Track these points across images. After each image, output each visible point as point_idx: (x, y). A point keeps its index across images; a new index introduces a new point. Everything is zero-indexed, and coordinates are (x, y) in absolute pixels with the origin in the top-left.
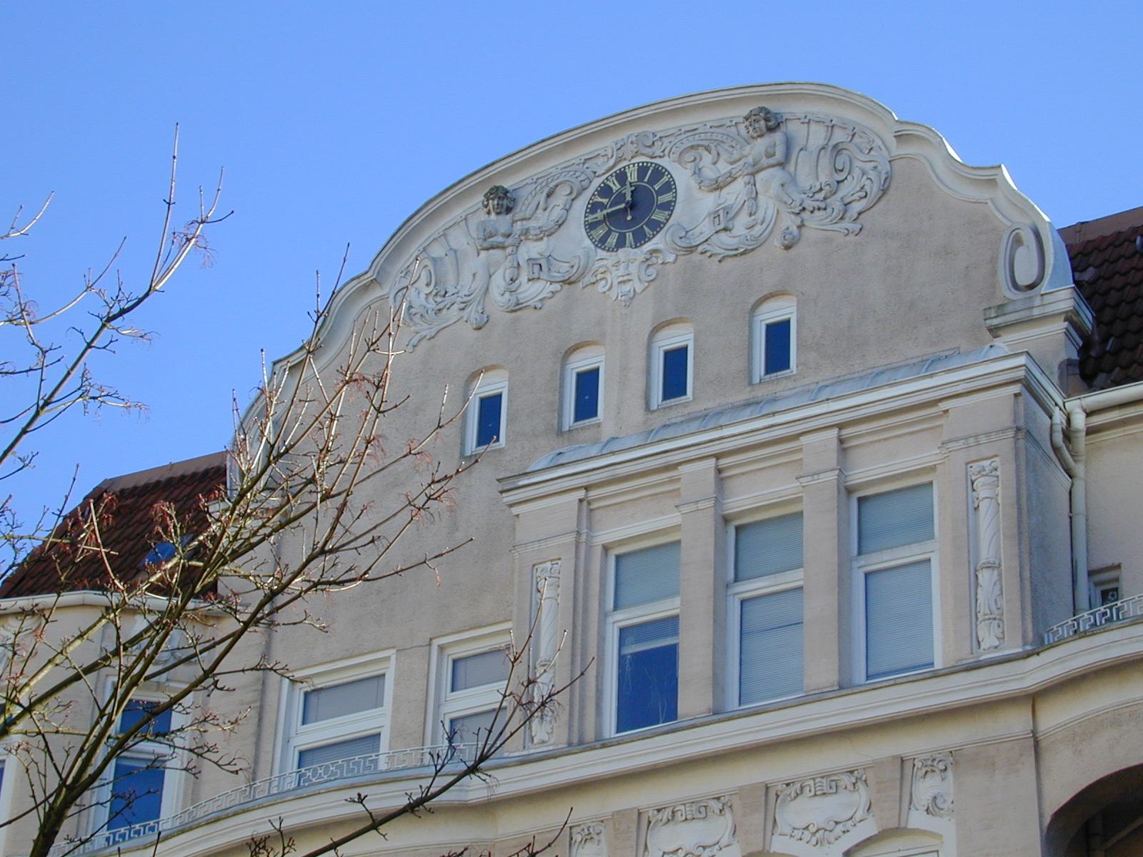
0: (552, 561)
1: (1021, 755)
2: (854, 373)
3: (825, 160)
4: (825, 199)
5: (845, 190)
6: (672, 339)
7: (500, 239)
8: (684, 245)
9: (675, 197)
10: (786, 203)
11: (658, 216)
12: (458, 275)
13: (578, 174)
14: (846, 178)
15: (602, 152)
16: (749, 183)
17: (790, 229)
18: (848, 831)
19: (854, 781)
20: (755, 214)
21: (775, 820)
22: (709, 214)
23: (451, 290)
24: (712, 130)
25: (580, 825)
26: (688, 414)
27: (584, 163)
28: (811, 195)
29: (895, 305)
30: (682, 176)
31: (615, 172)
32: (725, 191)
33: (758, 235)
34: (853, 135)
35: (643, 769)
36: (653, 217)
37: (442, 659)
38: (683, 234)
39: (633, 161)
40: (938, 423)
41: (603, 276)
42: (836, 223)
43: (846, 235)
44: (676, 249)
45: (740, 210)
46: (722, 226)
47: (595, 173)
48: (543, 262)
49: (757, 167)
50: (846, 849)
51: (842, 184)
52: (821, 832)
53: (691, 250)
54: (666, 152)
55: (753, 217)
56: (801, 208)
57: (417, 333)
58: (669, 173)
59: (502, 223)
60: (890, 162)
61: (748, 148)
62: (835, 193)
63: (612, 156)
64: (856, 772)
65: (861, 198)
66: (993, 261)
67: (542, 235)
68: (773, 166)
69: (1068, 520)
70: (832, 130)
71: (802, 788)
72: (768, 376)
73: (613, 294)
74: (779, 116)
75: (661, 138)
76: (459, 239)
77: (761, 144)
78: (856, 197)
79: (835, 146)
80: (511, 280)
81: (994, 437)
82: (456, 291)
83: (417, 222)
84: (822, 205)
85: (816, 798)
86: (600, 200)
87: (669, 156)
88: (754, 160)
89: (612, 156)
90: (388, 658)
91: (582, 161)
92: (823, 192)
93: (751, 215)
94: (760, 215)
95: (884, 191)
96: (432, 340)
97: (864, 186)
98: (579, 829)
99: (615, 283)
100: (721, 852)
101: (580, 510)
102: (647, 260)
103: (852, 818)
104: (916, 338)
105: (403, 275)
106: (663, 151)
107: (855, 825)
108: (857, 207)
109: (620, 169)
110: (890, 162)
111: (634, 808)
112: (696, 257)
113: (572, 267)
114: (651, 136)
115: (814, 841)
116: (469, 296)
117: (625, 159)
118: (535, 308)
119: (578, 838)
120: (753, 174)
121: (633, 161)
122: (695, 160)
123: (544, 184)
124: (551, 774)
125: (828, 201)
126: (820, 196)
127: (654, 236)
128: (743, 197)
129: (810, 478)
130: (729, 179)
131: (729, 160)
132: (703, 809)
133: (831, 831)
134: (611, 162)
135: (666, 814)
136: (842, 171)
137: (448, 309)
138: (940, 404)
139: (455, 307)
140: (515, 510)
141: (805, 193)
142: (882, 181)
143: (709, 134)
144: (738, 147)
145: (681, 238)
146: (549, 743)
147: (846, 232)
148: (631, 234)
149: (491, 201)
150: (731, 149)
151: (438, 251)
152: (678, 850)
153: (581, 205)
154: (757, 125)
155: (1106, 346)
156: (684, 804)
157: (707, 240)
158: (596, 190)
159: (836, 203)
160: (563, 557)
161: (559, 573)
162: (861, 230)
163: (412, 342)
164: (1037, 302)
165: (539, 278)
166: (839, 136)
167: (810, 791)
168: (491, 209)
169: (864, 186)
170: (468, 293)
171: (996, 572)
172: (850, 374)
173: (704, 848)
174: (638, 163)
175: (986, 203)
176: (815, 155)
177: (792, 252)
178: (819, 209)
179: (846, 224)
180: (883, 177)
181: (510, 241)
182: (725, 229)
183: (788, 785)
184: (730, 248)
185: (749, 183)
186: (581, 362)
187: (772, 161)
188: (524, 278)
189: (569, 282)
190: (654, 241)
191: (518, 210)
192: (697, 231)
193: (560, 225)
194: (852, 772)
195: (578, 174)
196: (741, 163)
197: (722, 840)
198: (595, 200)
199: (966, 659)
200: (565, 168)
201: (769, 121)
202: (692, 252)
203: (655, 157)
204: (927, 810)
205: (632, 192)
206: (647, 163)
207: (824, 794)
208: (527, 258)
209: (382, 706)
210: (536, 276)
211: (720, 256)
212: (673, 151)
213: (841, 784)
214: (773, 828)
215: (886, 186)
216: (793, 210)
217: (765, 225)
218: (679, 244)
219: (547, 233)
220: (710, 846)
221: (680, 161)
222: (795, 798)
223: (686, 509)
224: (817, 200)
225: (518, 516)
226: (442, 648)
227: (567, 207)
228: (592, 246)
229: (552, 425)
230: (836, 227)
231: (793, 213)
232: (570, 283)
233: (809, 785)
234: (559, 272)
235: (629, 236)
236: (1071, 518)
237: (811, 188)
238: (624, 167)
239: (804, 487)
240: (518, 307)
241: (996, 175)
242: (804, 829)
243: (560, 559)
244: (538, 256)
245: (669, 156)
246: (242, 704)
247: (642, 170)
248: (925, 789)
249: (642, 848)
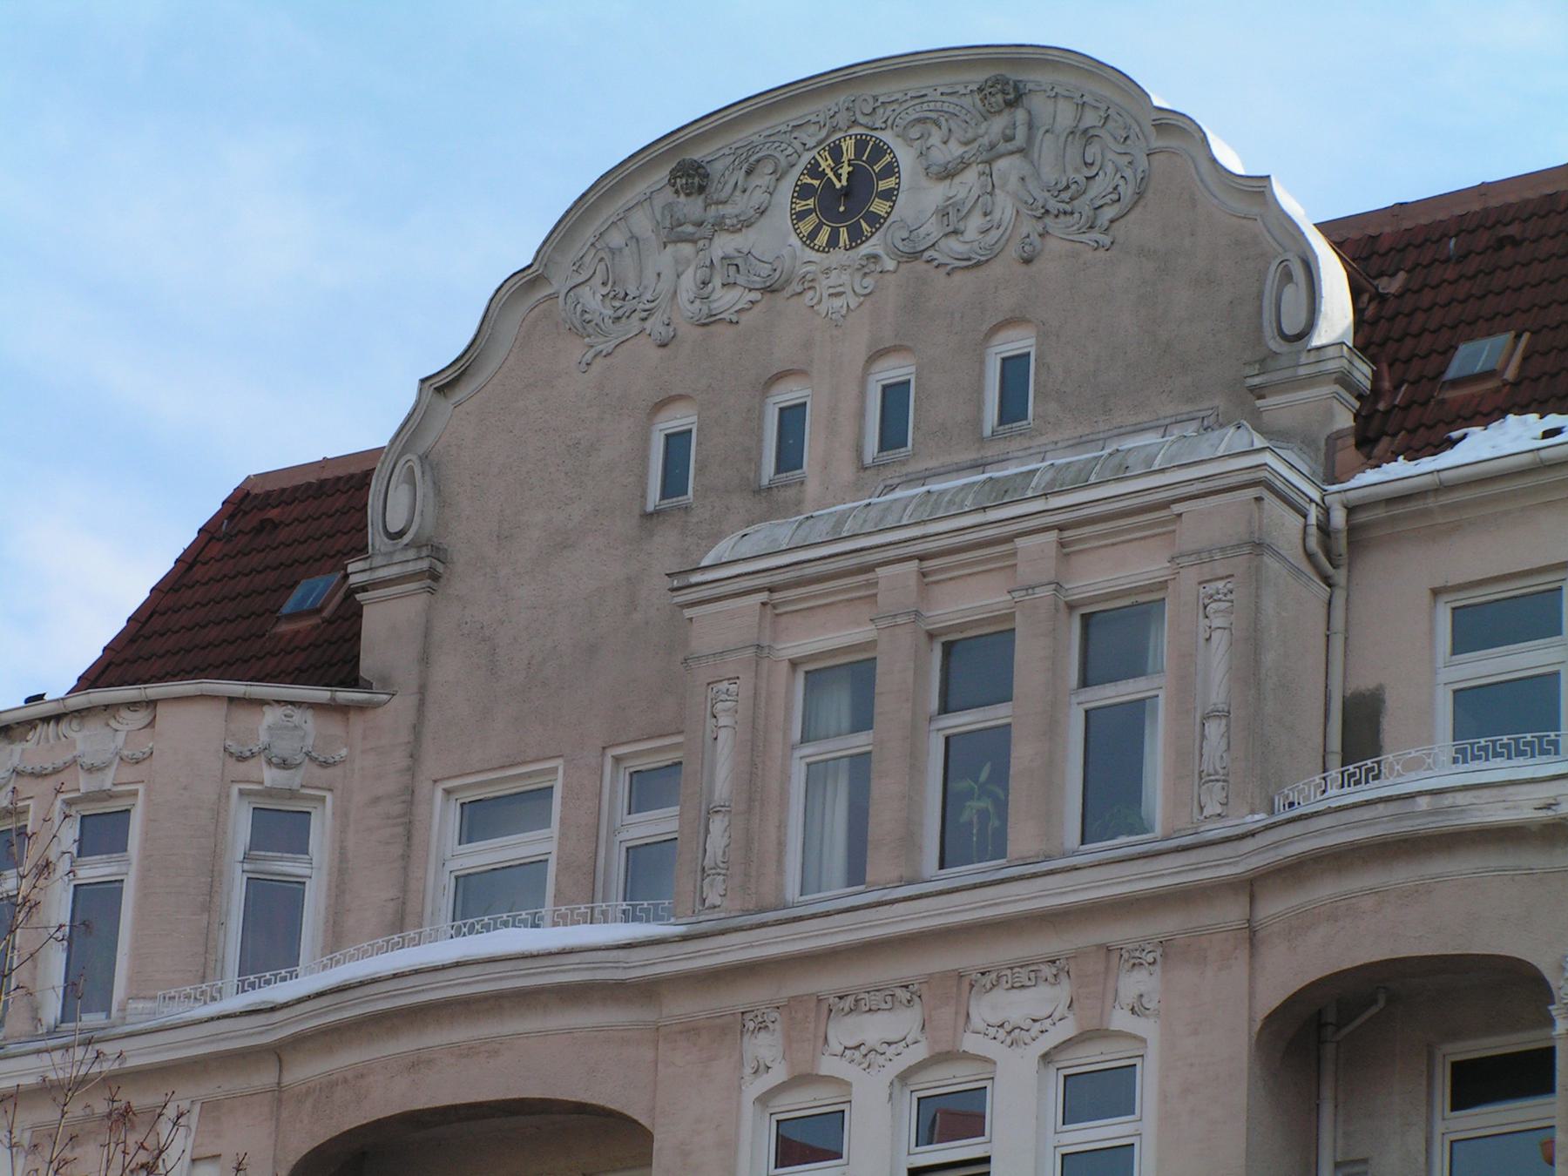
0: (729, 679)
1: (1236, 949)
2: (1099, 432)
3: (1073, 152)
4: (1072, 199)
5: (1097, 188)
6: (894, 370)
7: (689, 229)
8: (906, 250)
9: (899, 184)
10: (1026, 203)
11: (879, 207)
12: (641, 271)
13: (784, 146)
14: (1097, 174)
15: (813, 118)
16: (984, 173)
17: (1031, 237)
18: (1047, 1031)
19: (1055, 973)
20: (990, 213)
21: (968, 1014)
22: (937, 211)
23: (632, 292)
24: (944, 98)
25: (753, 1011)
26: (906, 475)
27: (791, 132)
28: (1056, 194)
29: (1148, 347)
30: (905, 157)
31: (829, 145)
32: (957, 180)
33: (993, 242)
34: (1107, 118)
35: (1316, 287)
36: (871, 209)
37: (618, 772)
38: (905, 235)
39: (851, 132)
40: (1170, 528)
41: (810, 284)
42: (1084, 232)
43: (1096, 249)
44: (897, 254)
45: (973, 207)
46: (951, 229)
47: (805, 145)
48: (739, 261)
49: (993, 153)
50: (1042, 1052)
51: (1092, 182)
52: (1017, 1031)
53: (915, 255)
54: (889, 123)
55: (988, 218)
56: (1043, 211)
57: (592, 346)
58: (892, 151)
59: (692, 207)
60: (1148, 155)
61: (984, 126)
62: (1084, 192)
63: (825, 125)
64: (1058, 962)
65: (1114, 202)
66: (1260, 296)
67: (739, 226)
68: (1012, 153)
69: (1324, 639)
70: (1082, 109)
71: (999, 977)
72: (1001, 428)
73: (822, 309)
74: (1021, 86)
75: (883, 103)
76: (642, 222)
77: (998, 124)
78: (1107, 200)
79: (1085, 131)
80: (703, 283)
81: (1230, 553)
82: (637, 293)
83: (592, 200)
84: (1068, 208)
85: (1014, 991)
86: (809, 181)
87: (892, 128)
88: (990, 142)
89: (825, 125)
90: (554, 770)
91: (789, 129)
92: (1070, 190)
93: (986, 214)
94: (997, 215)
95: (1140, 195)
96: (608, 358)
97: (1117, 186)
98: (751, 1016)
99: (825, 296)
100: (906, 1050)
101: (762, 617)
102: (863, 266)
103: (1050, 1016)
104: (1171, 392)
105: (575, 268)
106: (885, 122)
107: (1054, 1024)
108: (1109, 213)
109: (834, 142)
110: (1148, 155)
111: (813, 994)
112: (920, 266)
113: (775, 270)
114: (871, 101)
115: (1009, 1041)
116: (653, 301)
117: (840, 129)
118: (731, 322)
119: (751, 1025)
120: (989, 162)
121: (851, 132)
122: (922, 136)
123: (743, 157)
124: (717, 953)
125: (1075, 203)
126: (1065, 196)
127: (873, 234)
128: (975, 192)
129: (1024, 592)
130: (961, 166)
131: (962, 139)
132: (889, 999)
133: (1028, 1031)
134: (823, 133)
135: (849, 1001)
136: (1092, 164)
137: (628, 317)
138: (1172, 506)
139: (636, 316)
140: (688, 613)
141: (1049, 191)
142: (1138, 181)
143: (939, 104)
144: (973, 123)
145: (903, 240)
146: (721, 908)
147: (1096, 245)
148: (845, 229)
149: (678, 180)
150: (964, 125)
151: (616, 238)
152: (861, 1045)
153: (787, 187)
154: (993, 100)
155: (1395, 399)
156: (868, 992)
157: (933, 245)
158: (806, 168)
159: (1083, 204)
160: (740, 676)
161: (737, 695)
162: (1112, 243)
163: (584, 360)
164: (1304, 359)
165: (735, 283)
166: (1090, 119)
167: (1007, 982)
168: (679, 189)
169: (1117, 186)
170: (651, 298)
171: (1224, 721)
172: (1092, 433)
173: (889, 1044)
174: (856, 135)
175: (1256, 220)
176: (1062, 139)
177: (1034, 268)
178: (1065, 213)
179: (1095, 235)
180: (1140, 176)
181: (700, 232)
182: (955, 232)
183: (983, 974)
184: (959, 257)
185: (984, 173)
186: (789, 393)
187: (1010, 146)
188: (717, 281)
189: (770, 290)
190: (873, 241)
191: (713, 190)
192: (922, 231)
193: (763, 213)
194: (1054, 962)
195: (784, 146)
196: (976, 145)
197: (908, 1036)
198: (805, 181)
199: (1184, 829)
200: (770, 136)
201: (1008, 94)
202: (916, 259)
203: (876, 129)
204: (1132, 1009)
205: (849, 173)
206: (867, 135)
207: (1023, 986)
208: (722, 255)
209: (549, 827)
210: (731, 280)
211: (949, 268)
212: (901, 115)
213: (1043, 974)
214: (966, 1023)
215: (1142, 187)
216: (1034, 213)
217: (1002, 229)
218: (901, 249)
219: (745, 224)
220: (896, 1043)
221: (902, 135)
222: (991, 989)
223: (883, 624)
224: (1063, 202)
225: (691, 619)
226: (617, 760)
227: (771, 189)
228: (799, 243)
229: (748, 479)
230: (1084, 238)
231: (1035, 216)
232: (773, 291)
233: (1006, 975)
234: (759, 276)
235: (844, 236)
236: (1328, 636)
237: (1056, 184)
238: (840, 139)
239: (1016, 602)
240: (709, 321)
241: (1265, 187)
242: (998, 1027)
243: (738, 678)
244: (736, 254)
245: (892, 128)
246: (389, 818)
247: (861, 144)
248: (1134, 983)
249: (821, 1040)
